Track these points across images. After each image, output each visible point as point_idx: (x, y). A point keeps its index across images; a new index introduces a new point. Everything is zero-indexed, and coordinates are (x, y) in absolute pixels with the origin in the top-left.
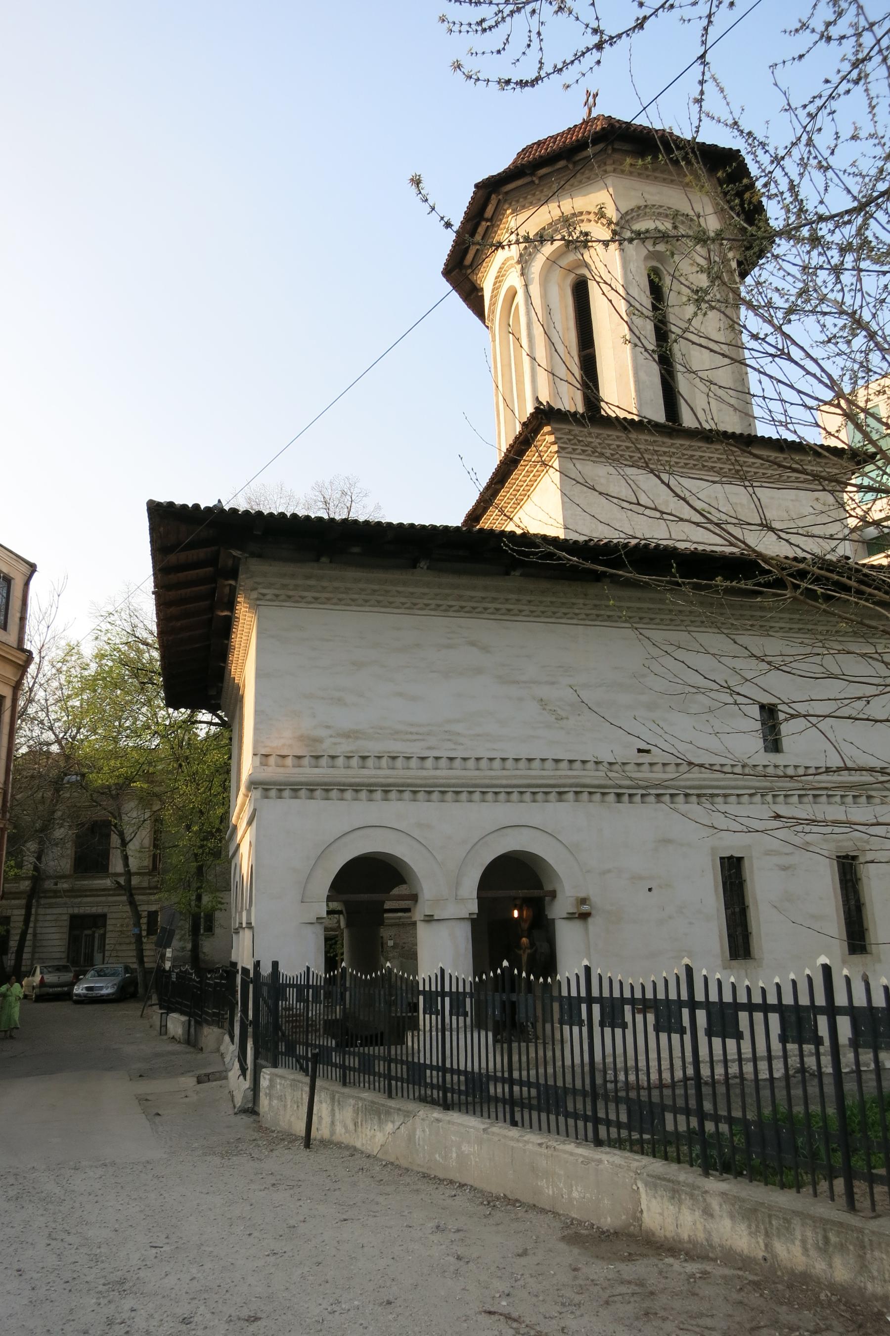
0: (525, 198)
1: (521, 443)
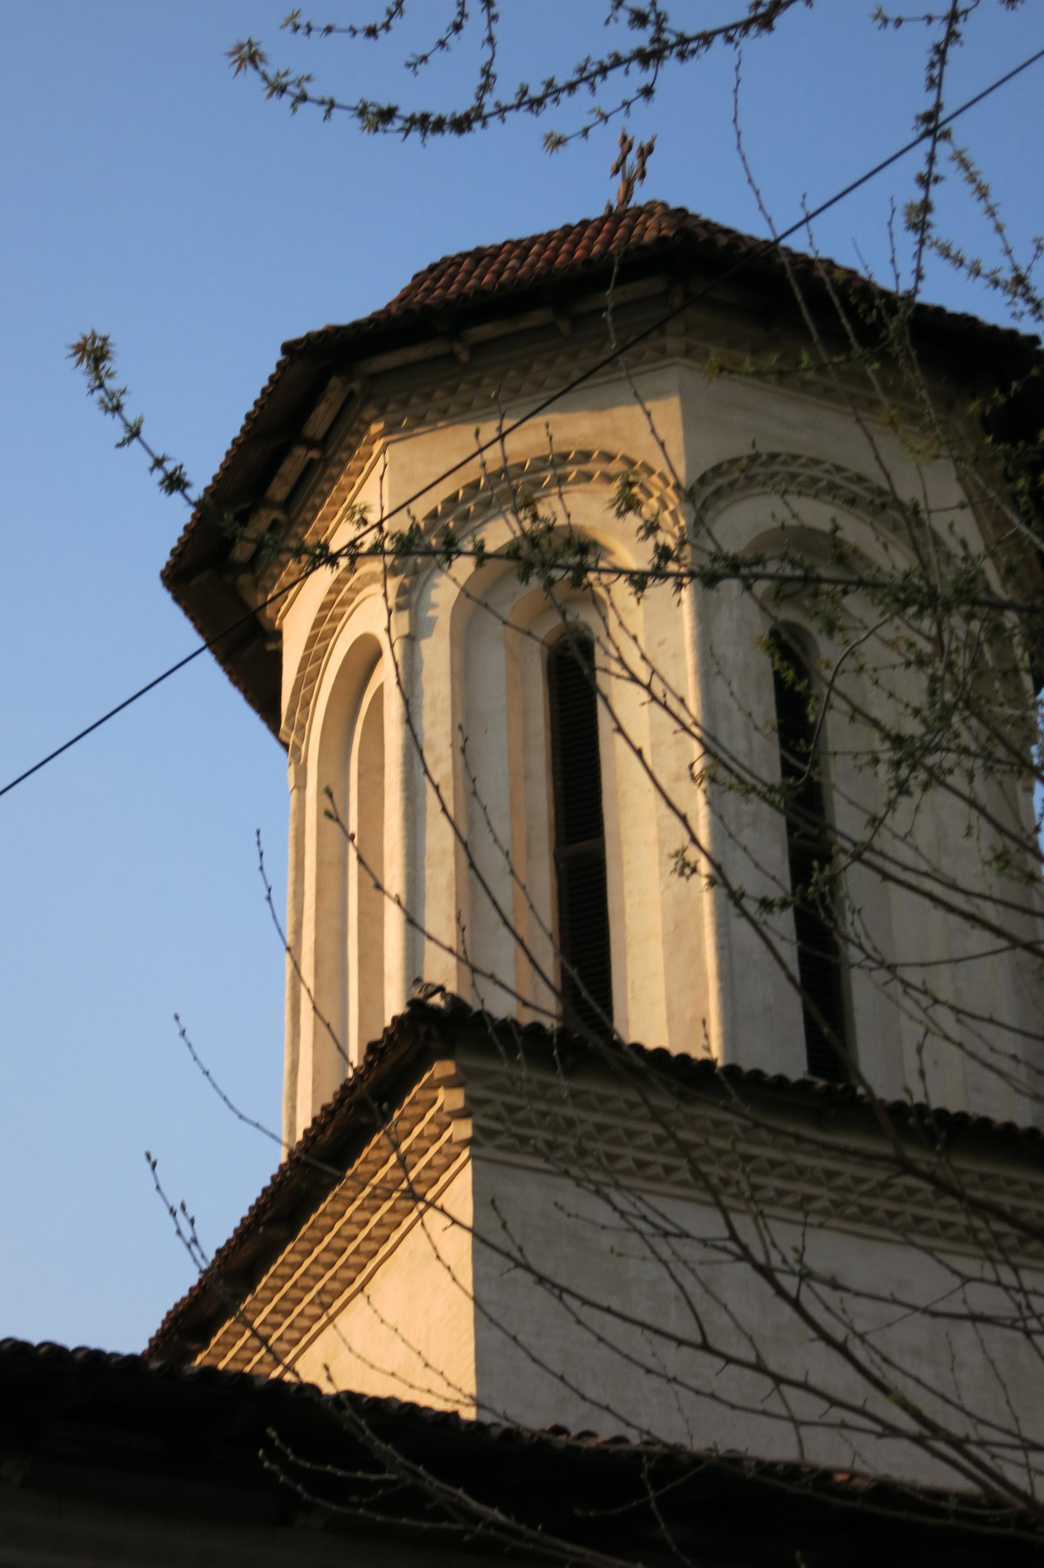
0: (428, 397)
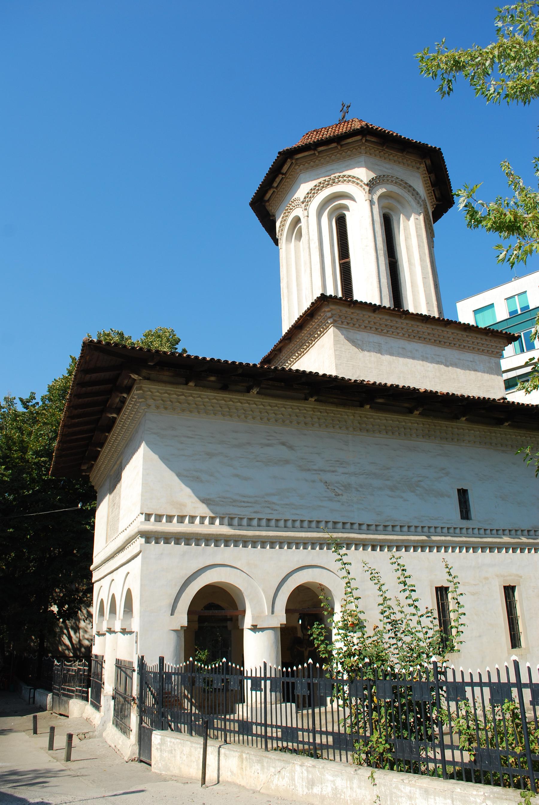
1: (307, 315)
